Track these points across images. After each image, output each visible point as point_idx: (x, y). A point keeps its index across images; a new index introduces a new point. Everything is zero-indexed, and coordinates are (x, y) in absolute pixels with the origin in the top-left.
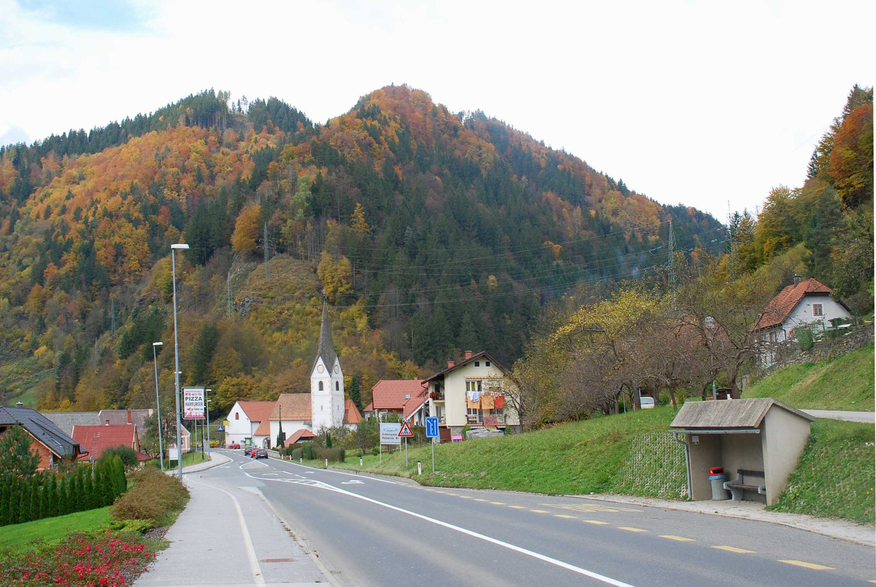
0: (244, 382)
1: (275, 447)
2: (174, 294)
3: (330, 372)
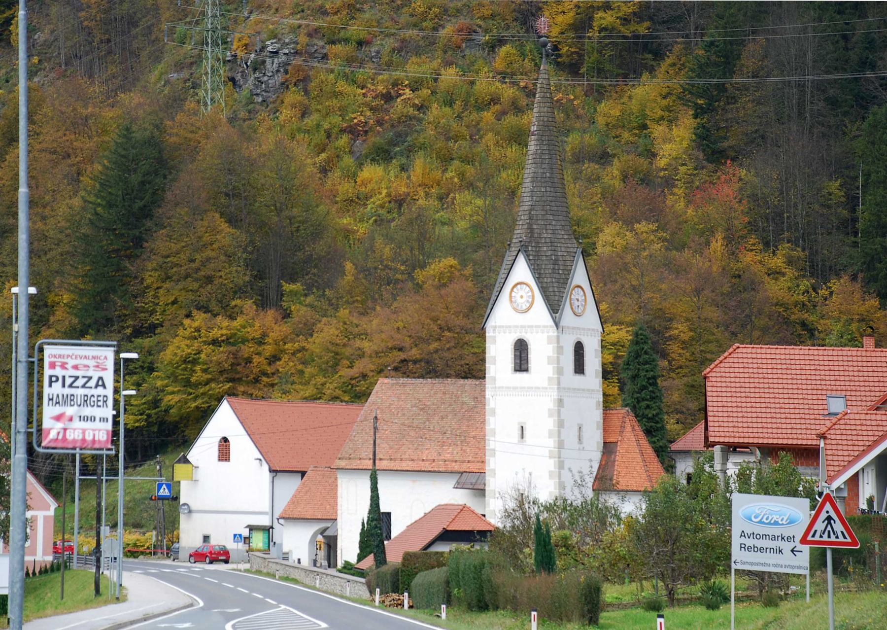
0: (254, 332)
1: (353, 559)
2: (21, 13)
3: (554, 307)
